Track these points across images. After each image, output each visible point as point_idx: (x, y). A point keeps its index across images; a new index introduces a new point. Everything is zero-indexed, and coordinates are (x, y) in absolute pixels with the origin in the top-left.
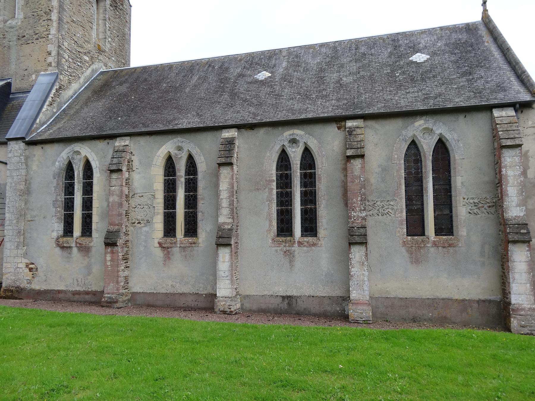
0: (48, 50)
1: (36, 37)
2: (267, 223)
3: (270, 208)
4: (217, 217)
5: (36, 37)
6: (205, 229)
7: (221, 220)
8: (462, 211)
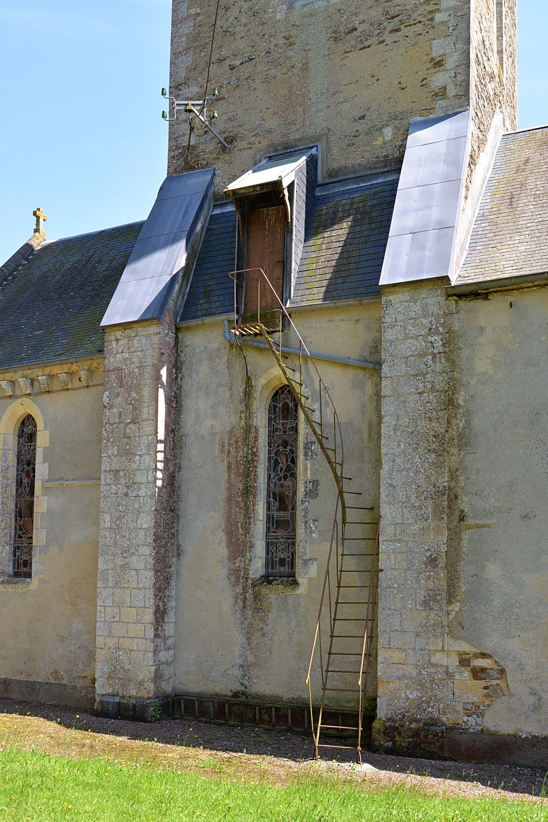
0: (434, 54)
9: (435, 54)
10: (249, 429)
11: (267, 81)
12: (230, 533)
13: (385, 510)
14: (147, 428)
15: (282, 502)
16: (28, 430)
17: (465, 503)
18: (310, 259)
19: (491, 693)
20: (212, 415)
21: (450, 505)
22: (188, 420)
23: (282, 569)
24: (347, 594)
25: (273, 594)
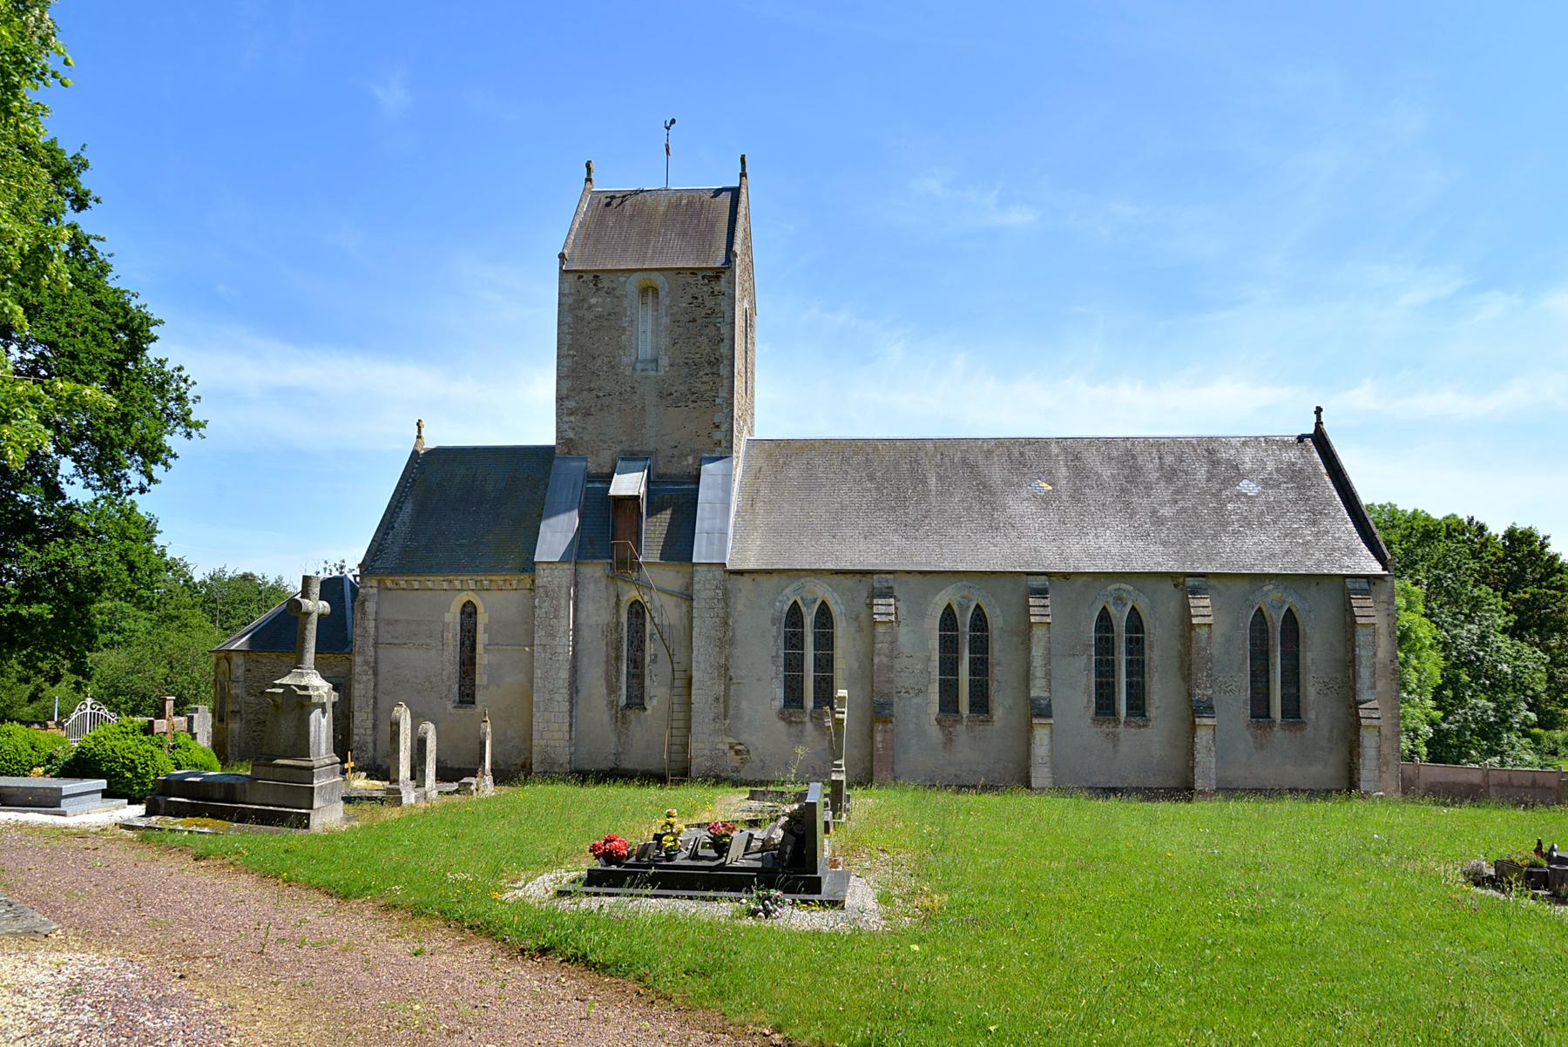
1: (693, 397)
2: (1085, 699)
3: (1089, 680)
4: (1028, 689)
5: (693, 397)
6: (1002, 702)
7: (1034, 693)
8: (1311, 690)
9: (716, 420)
10: (618, 623)
11: (619, 410)
12: (608, 681)
13: (695, 674)
14: (564, 622)
15: (636, 664)
16: (469, 610)
17: (732, 672)
18: (654, 529)
19: (744, 761)
20: (597, 613)
21: (725, 673)
22: (582, 616)
23: (637, 701)
24: (676, 716)
25: (632, 715)
